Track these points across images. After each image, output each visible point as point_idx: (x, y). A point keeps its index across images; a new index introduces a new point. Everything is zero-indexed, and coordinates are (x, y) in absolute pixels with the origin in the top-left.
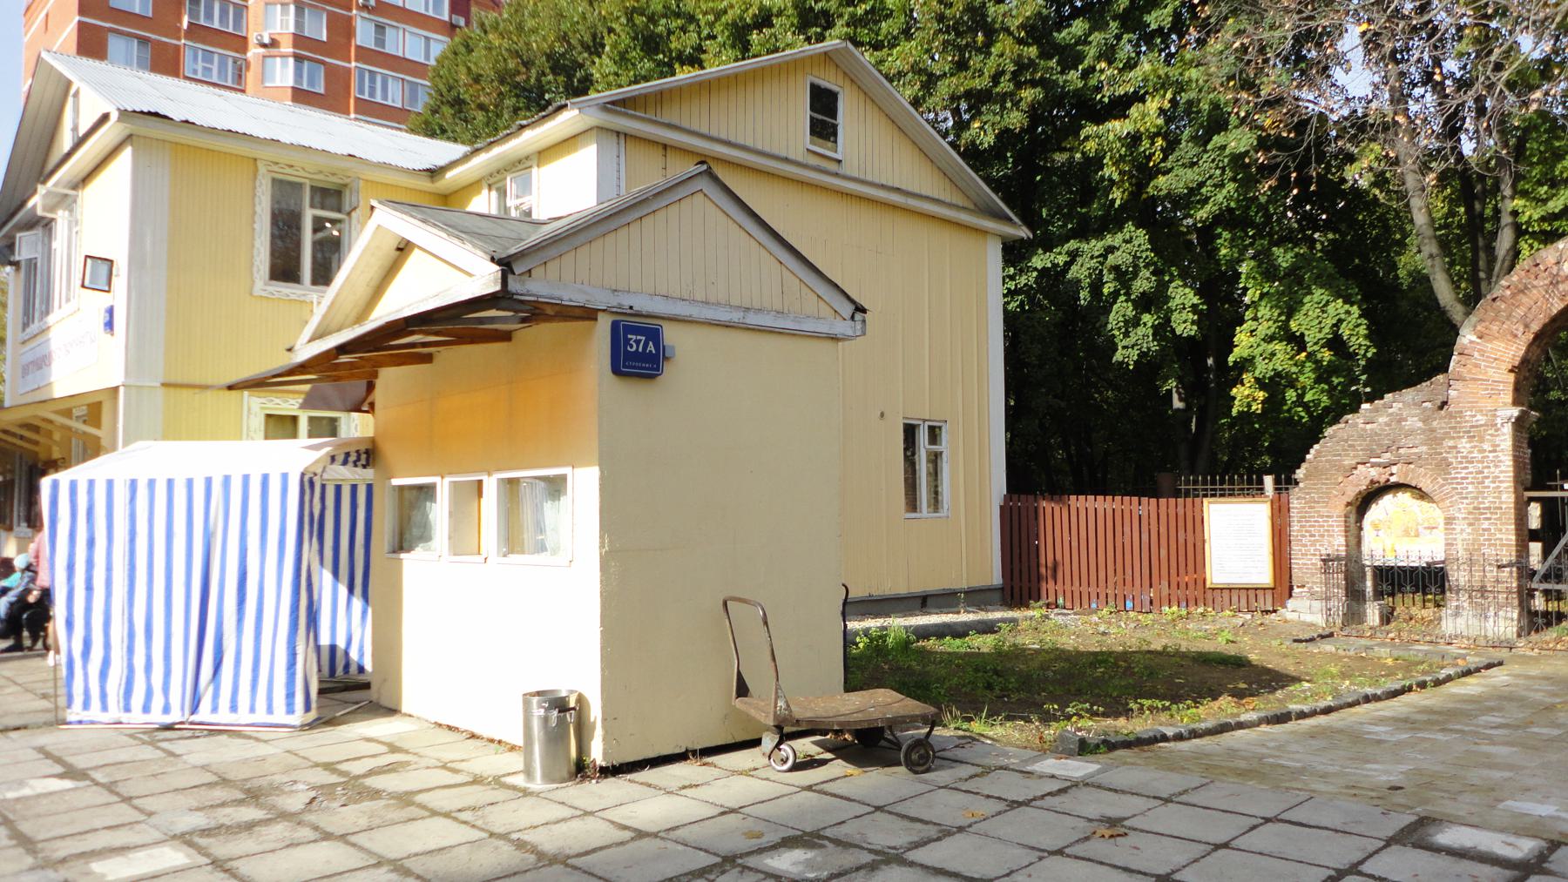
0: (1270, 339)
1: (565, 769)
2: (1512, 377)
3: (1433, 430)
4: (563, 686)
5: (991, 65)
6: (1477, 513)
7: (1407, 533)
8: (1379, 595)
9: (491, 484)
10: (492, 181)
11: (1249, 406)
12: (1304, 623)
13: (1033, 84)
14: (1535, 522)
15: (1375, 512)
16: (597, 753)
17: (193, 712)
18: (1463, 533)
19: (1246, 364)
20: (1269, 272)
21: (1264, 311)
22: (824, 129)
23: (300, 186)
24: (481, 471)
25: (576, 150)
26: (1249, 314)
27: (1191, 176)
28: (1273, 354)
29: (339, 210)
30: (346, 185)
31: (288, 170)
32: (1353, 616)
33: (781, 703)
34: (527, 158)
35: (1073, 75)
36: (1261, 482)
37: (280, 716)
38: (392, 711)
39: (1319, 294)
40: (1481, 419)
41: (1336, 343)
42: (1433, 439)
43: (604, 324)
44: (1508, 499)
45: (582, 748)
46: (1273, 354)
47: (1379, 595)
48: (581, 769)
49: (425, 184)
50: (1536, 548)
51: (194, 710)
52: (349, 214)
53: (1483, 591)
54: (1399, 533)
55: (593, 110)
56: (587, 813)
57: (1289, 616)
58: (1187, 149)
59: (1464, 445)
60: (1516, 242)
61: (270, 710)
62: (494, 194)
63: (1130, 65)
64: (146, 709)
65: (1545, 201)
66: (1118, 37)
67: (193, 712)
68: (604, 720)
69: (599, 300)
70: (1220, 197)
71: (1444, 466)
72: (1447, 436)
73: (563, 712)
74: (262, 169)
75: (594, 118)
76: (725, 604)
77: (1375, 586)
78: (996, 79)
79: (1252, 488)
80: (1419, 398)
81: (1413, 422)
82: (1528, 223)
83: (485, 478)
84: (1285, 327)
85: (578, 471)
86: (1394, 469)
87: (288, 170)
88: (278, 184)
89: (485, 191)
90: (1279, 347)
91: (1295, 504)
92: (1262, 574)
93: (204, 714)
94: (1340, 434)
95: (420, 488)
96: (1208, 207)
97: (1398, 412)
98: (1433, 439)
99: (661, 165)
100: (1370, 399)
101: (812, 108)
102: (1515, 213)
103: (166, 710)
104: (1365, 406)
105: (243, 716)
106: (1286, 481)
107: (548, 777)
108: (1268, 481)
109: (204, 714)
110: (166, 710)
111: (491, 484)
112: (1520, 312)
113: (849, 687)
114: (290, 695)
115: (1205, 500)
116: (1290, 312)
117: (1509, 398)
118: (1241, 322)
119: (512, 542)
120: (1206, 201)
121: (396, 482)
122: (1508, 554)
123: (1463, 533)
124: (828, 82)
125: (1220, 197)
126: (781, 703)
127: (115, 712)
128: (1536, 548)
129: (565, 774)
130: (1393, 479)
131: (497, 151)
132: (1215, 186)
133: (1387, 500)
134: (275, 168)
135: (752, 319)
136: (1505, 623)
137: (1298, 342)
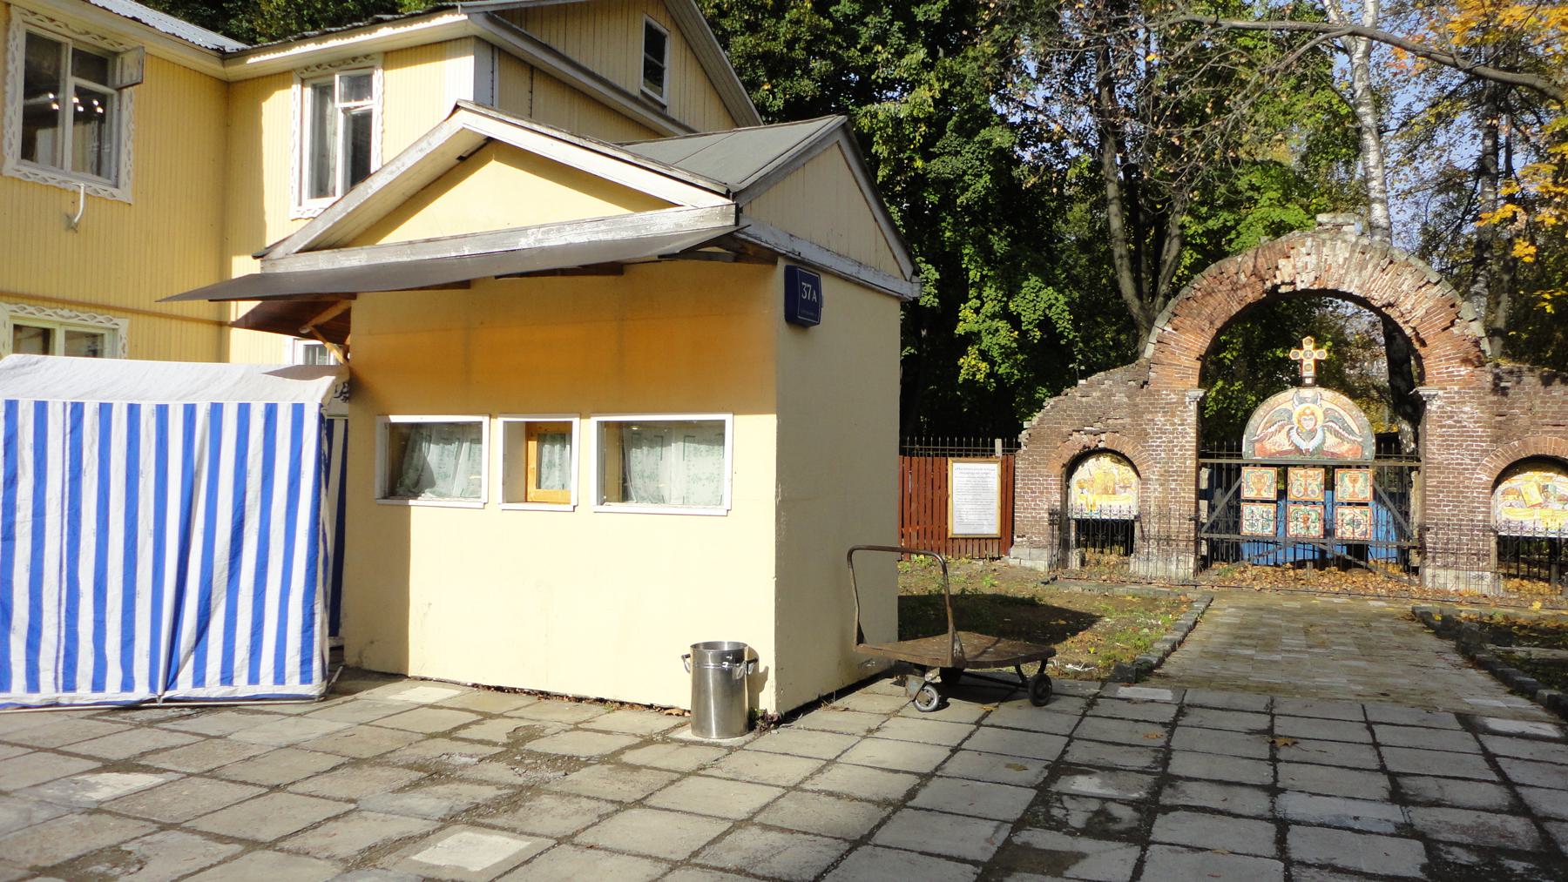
0: (993, 317)
1: (741, 722)
2: (1198, 365)
3: (1136, 405)
4: (727, 637)
5: (784, 29)
6: (1166, 475)
7: (1106, 491)
8: (1078, 544)
9: (586, 431)
10: (306, 75)
11: (974, 375)
12: (1025, 568)
13: (823, 55)
14: (1204, 485)
15: (1081, 473)
16: (768, 702)
17: (166, 688)
18: (1155, 492)
19: (972, 338)
20: (986, 254)
21: (989, 292)
22: (654, 73)
23: (57, 46)
24: (572, 412)
25: (442, 58)
26: (972, 292)
27: (957, 163)
28: (997, 330)
29: (104, 83)
30: (116, 54)
31: (47, 24)
32: (1063, 562)
33: (957, 647)
34: (367, 56)
35: (854, 52)
36: (993, 445)
37: (293, 686)
38: (398, 675)
39: (1034, 281)
40: (1174, 397)
41: (1046, 324)
42: (1136, 413)
43: (781, 265)
44: (1191, 463)
45: (754, 700)
46: (997, 330)
47: (1078, 544)
48: (754, 721)
49: (214, 67)
50: (1204, 504)
51: (170, 683)
52: (119, 90)
53: (1168, 540)
54: (1103, 491)
55: (480, 19)
56: (276, 788)
57: (1012, 562)
58: (950, 138)
59: (1160, 418)
60: (1180, 252)
61: (279, 678)
62: (308, 91)
63: (900, 53)
64: (98, 685)
65: (1205, 220)
66: (891, 23)
67: (166, 688)
68: (779, 669)
69: (783, 245)
70: (979, 186)
71: (1142, 436)
72: (1147, 410)
73: (728, 671)
74: (16, 18)
75: (481, 27)
76: (850, 553)
77: (1077, 534)
78: (790, 44)
79: (986, 453)
80: (1128, 376)
81: (1121, 398)
82: (1192, 236)
83: (576, 421)
84: (1005, 308)
85: (740, 419)
86: (1103, 437)
87: (47, 24)
88: (32, 39)
89: (296, 88)
90: (1001, 324)
91: (1020, 464)
92: (991, 527)
93: (184, 686)
94: (1061, 405)
95: (469, 424)
96: (968, 194)
97: (1100, 391)
98: (1136, 413)
99: (528, 88)
100: (1084, 375)
101: (647, 50)
102: (1182, 227)
103: (127, 684)
104: (1082, 382)
105: (241, 687)
106: (1012, 446)
107: (726, 731)
108: (998, 442)
109: (184, 686)
110: (127, 684)
111: (586, 431)
112: (1208, 310)
113: (902, 636)
114: (306, 662)
115: (950, 460)
116: (1010, 295)
117: (1196, 381)
118: (966, 300)
119: (516, 490)
120: (965, 189)
121: (394, 419)
122: (1188, 510)
123: (1155, 492)
124: (661, 25)
125: (979, 186)
126: (957, 647)
127: (48, 689)
128: (1204, 504)
129: (742, 727)
130: (1101, 445)
131: (333, 43)
132: (976, 175)
133: (1092, 462)
134: (33, 19)
135: (866, 276)
136: (1184, 566)
137: (1014, 321)
